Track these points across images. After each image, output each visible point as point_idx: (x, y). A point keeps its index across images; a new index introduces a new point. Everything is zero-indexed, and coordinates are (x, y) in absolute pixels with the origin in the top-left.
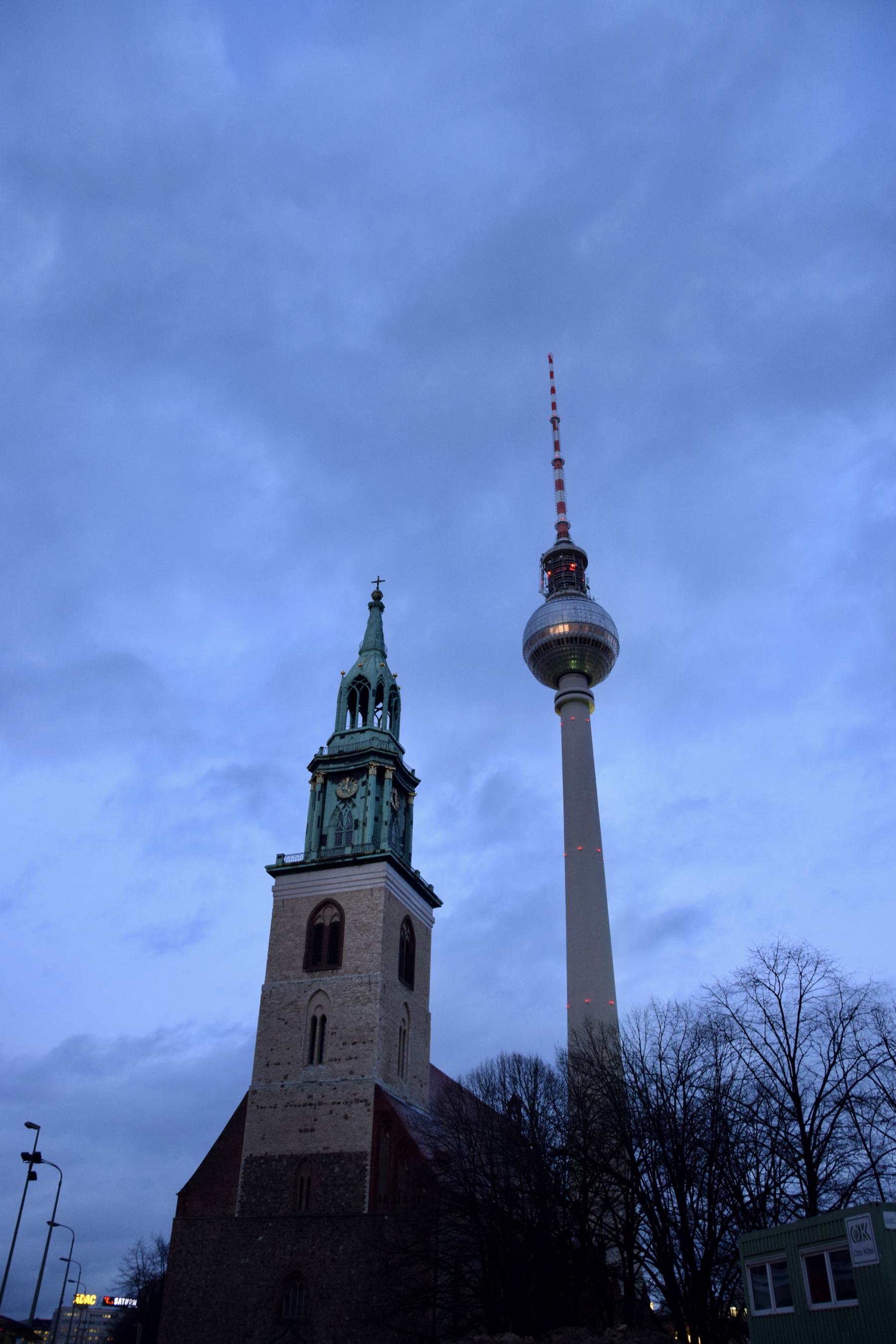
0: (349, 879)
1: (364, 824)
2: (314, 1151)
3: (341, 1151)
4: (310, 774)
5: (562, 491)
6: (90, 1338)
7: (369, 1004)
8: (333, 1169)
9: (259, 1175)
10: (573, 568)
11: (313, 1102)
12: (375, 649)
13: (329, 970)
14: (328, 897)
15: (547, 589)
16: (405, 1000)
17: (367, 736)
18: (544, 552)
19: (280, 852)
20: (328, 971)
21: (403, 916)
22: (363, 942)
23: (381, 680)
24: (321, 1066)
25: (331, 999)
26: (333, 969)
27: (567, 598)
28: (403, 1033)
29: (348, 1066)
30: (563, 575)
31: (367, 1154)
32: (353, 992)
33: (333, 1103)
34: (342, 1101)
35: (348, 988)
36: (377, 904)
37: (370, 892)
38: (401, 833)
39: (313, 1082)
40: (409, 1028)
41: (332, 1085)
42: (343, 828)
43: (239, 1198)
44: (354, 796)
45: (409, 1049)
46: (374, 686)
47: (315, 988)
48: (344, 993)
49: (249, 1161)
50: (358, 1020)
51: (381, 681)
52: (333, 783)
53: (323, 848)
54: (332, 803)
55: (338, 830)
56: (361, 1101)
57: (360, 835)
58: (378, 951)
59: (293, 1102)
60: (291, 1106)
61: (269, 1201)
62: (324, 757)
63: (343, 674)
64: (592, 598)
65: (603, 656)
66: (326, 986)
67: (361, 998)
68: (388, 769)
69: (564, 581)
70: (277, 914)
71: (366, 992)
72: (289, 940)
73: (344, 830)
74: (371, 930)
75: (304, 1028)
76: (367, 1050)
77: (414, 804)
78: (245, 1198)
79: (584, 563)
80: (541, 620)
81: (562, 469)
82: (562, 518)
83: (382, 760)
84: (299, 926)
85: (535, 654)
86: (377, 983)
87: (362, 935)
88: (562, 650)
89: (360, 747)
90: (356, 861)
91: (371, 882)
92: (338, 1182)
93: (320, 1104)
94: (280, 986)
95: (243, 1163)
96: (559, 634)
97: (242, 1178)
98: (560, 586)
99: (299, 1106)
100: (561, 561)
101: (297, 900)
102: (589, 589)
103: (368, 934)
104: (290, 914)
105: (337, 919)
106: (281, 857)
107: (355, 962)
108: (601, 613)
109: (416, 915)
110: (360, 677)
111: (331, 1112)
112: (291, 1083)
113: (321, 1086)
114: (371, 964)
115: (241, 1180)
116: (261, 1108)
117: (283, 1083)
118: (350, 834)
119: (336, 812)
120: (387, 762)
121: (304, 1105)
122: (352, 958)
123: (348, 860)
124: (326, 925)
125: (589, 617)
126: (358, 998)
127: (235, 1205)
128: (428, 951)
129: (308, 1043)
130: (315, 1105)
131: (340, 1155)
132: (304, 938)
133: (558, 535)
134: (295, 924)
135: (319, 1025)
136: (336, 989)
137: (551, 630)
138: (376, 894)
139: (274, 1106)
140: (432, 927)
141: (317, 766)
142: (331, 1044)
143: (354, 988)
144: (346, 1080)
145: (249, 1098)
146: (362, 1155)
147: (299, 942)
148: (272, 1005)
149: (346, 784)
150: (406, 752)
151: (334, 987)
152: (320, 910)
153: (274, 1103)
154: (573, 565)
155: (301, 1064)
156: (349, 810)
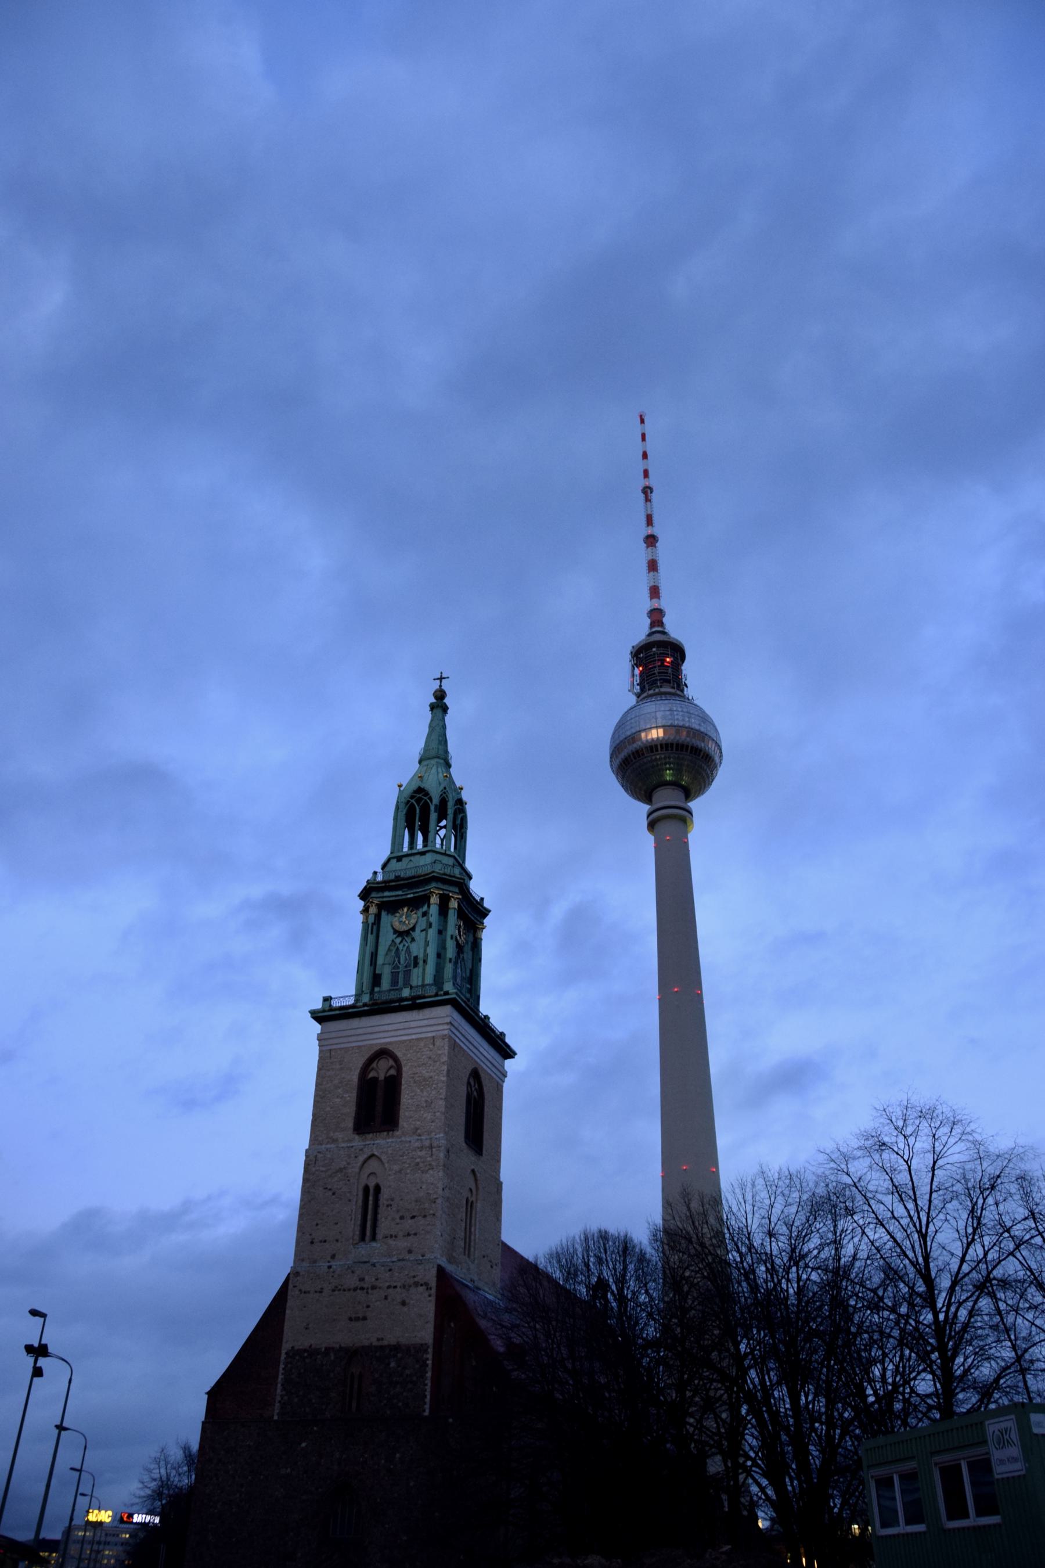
0: (407, 1025)
1: (425, 962)
2: (366, 1343)
3: (398, 1343)
4: (362, 903)
5: (655, 573)
6: (105, 1561)
7: (431, 1172)
8: (389, 1364)
9: (302, 1371)
10: (668, 663)
11: (365, 1286)
12: (438, 757)
13: (384, 1131)
14: (383, 1047)
15: (638, 687)
16: (473, 1167)
17: (428, 858)
18: (635, 644)
19: (327, 995)
20: (382, 1133)
21: (470, 1068)
22: (423, 1099)
23: (445, 793)
24: (374, 1244)
25: (386, 1165)
26: (388, 1131)
27: (661, 697)
28: (470, 1205)
29: (406, 1244)
30: (656, 671)
31: (428, 1347)
32: (412, 1158)
33: (389, 1287)
34: (399, 1284)
35: (406, 1152)
36: (440, 1055)
37: (432, 1041)
38: (468, 971)
39: (365, 1262)
40: (477, 1200)
41: (387, 1265)
42: (401, 966)
43: (278, 1398)
44: (413, 929)
45: (477, 1233)
46: (436, 800)
47: (367, 1152)
48: (401, 1158)
49: (291, 1354)
50: (418, 1190)
51: (444, 795)
52: (388, 914)
53: (377, 989)
54: (387, 937)
55: (394, 968)
56: (422, 1285)
57: (420, 974)
58: (441, 1110)
59: (342, 1286)
60: (340, 1290)
61: (314, 1401)
62: (378, 883)
63: (400, 786)
64: (690, 698)
65: (703, 765)
66: (381, 1150)
67: (421, 1165)
68: (453, 897)
69: (658, 678)
70: (323, 1066)
71: (426, 1158)
72: (337, 1097)
73: (401, 969)
74: (432, 1084)
75: (355, 1200)
76: (429, 1224)
77: (483, 938)
78: (286, 1398)
79: (681, 657)
80: (631, 723)
81: (656, 547)
82: (655, 604)
83: (445, 887)
84: (349, 1081)
85: (624, 763)
86: (439, 1147)
87: (422, 1091)
88: (656, 759)
89: (420, 872)
90: (415, 1004)
91: (433, 1029)
92: (395, 1379)
93: (374, 1288)
94: (327, 1150)
95: (283, 1356)
96: (653, 739)
97: (282, 1374)
98: (653, 684)
99: (349, 1290)
100: (654, 654)
101: (346, 1050)
102: (687, 687)
103: (429, 1089)
104: (338, 1067)
105: (393, 1072)
106: (328, 999)
107: (414, 1123)
108: (701, 715)
109: (485, 1067)
110: (420, 790)
111: (386, 1298)
112: (339, 1263)
113: (375, 1266)
114: (433, 1124)
115: (281, 1377)
116: (305, 1292)
117: (331, 1264)
118: (408, 973)
119: (392, 948)
120: (452, 888)
121: (355, 1289)
122: (411, 1117)
123: (406, 1003)
124: (380, 1079)
125: (687, 719)
126: (418, 1164)
127: (274, 1405)
128: (499, 1109)
129: (359, 1217)
130: (368, 1289)
131: (396, 1348)
132: (354, 1095)
133: (651, 624)
134: (344, 1078)
135: (371, 1195)
136: (392, 1154)
137: (643, 735)
138: (438, 1043)
139: (319, 1290)
140: (503, 1082)
141: (370, 894)
142: (386, 1218)
143: (413, 1153)
144: (403, 1260)
145: (290, 1281)
146: (422, 1348)
147: (348, 1098)
148: (317, 1173)
149: (403, 914)
150: (473, 877)
151: (390, 1152)
152: (374, 1061)
153: (320, 1287)
154: (668, 660)
155: (351, 1241)
156: (407, 945)
